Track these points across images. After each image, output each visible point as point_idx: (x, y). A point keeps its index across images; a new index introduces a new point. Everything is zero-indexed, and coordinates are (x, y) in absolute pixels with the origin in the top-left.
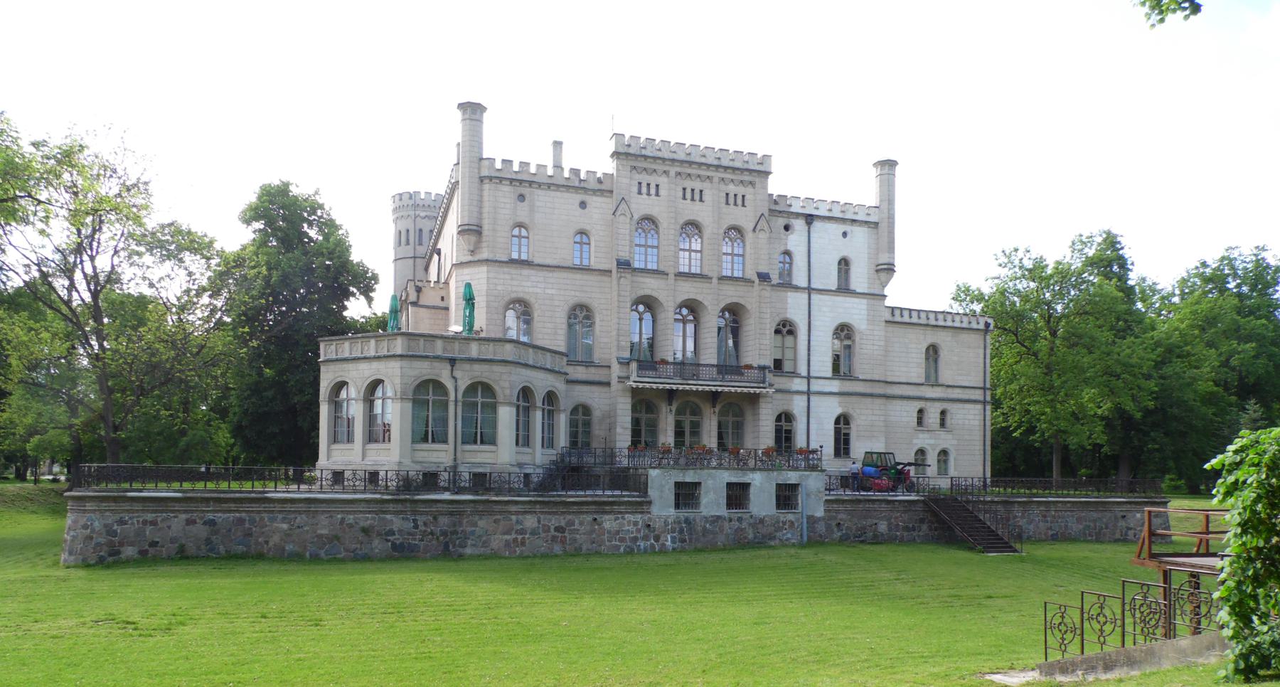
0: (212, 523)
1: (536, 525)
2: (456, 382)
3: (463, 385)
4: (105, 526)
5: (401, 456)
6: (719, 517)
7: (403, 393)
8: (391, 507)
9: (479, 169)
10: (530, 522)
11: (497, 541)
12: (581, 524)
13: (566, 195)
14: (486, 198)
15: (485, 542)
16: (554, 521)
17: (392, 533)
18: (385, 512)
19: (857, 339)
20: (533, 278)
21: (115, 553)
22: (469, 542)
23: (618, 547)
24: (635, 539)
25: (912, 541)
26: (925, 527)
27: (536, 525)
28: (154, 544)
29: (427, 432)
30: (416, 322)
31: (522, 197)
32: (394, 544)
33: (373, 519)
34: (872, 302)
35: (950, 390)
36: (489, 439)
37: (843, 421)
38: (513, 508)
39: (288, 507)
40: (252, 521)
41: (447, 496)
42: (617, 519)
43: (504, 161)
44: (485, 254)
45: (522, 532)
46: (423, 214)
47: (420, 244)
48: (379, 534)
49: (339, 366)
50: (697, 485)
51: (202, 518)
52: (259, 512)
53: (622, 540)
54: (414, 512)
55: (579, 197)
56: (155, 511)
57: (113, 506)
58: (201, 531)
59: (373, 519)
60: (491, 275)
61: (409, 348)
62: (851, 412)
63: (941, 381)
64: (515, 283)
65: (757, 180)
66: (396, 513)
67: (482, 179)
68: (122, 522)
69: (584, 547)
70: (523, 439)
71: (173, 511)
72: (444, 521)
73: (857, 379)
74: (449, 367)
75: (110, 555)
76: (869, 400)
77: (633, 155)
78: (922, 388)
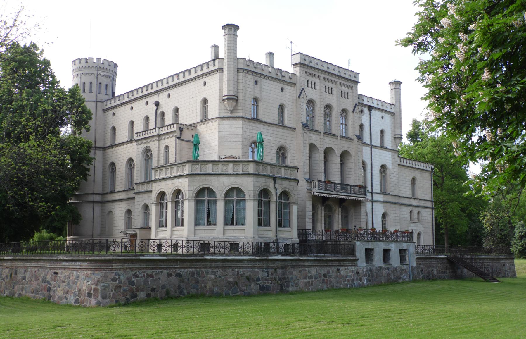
0: (179, 275)
1: (316, 273)
2: (220, 186)
3: (279, 192)
4: (128, 278)
5: (254, 234)
6: (381, 267)
7: (254, 196)
8: (258, 264)
9: (237, 63)
10: (313, 271)
11: (302, 282)
12: (333, 272)
13: (275, 83)
14: (240, 81)
15: (296, 284)
16: (323, 271)
17: (258, 279)
18: (255, 267)
19: (388, 173)
21: (135, 296)
22: (291, 284)
23: (347, 285)
24: (353, 280)
25: (444, 279)
26: (448, 271)
27: (316, 273)
28: (153, 290)
29: (233, 219)
30: (181, 150)
31: (256, 82)
32: (260, 286)
33: (250, 271)
34: (393, 154)
35: (420, 201)
38: (307, 264)
39: (214, 265)
40: (198, 273)
41: (279, 257)
42: (345, 269)
44: (240, 114)
45: (310, 277)
46: (102, 74)
47: (100, 93)
48: (254, 281)
50: (373, 249)
51: (174, 272)
52: (200, 268)
53: (348, 281)
54: (268, 267)
55: (281, 85)
56: (152, 269)
57: (131, 265)
58: (174, 280)
59: (250, 271)
60: (244, 126)
61: (256, 170)
62: (387, 212)
65: (353, 85)
66: (260, 267)
67: (238, 70)
68: (136, 276)
69: (335, 285)
70: (262, 220)
71: (161, 268)
72: (279, 271)
73: (389, 194)
74: (273, 182)
75: (132, 298)
76: (397, 206)
77: (308, 65)
78: (412, 200)
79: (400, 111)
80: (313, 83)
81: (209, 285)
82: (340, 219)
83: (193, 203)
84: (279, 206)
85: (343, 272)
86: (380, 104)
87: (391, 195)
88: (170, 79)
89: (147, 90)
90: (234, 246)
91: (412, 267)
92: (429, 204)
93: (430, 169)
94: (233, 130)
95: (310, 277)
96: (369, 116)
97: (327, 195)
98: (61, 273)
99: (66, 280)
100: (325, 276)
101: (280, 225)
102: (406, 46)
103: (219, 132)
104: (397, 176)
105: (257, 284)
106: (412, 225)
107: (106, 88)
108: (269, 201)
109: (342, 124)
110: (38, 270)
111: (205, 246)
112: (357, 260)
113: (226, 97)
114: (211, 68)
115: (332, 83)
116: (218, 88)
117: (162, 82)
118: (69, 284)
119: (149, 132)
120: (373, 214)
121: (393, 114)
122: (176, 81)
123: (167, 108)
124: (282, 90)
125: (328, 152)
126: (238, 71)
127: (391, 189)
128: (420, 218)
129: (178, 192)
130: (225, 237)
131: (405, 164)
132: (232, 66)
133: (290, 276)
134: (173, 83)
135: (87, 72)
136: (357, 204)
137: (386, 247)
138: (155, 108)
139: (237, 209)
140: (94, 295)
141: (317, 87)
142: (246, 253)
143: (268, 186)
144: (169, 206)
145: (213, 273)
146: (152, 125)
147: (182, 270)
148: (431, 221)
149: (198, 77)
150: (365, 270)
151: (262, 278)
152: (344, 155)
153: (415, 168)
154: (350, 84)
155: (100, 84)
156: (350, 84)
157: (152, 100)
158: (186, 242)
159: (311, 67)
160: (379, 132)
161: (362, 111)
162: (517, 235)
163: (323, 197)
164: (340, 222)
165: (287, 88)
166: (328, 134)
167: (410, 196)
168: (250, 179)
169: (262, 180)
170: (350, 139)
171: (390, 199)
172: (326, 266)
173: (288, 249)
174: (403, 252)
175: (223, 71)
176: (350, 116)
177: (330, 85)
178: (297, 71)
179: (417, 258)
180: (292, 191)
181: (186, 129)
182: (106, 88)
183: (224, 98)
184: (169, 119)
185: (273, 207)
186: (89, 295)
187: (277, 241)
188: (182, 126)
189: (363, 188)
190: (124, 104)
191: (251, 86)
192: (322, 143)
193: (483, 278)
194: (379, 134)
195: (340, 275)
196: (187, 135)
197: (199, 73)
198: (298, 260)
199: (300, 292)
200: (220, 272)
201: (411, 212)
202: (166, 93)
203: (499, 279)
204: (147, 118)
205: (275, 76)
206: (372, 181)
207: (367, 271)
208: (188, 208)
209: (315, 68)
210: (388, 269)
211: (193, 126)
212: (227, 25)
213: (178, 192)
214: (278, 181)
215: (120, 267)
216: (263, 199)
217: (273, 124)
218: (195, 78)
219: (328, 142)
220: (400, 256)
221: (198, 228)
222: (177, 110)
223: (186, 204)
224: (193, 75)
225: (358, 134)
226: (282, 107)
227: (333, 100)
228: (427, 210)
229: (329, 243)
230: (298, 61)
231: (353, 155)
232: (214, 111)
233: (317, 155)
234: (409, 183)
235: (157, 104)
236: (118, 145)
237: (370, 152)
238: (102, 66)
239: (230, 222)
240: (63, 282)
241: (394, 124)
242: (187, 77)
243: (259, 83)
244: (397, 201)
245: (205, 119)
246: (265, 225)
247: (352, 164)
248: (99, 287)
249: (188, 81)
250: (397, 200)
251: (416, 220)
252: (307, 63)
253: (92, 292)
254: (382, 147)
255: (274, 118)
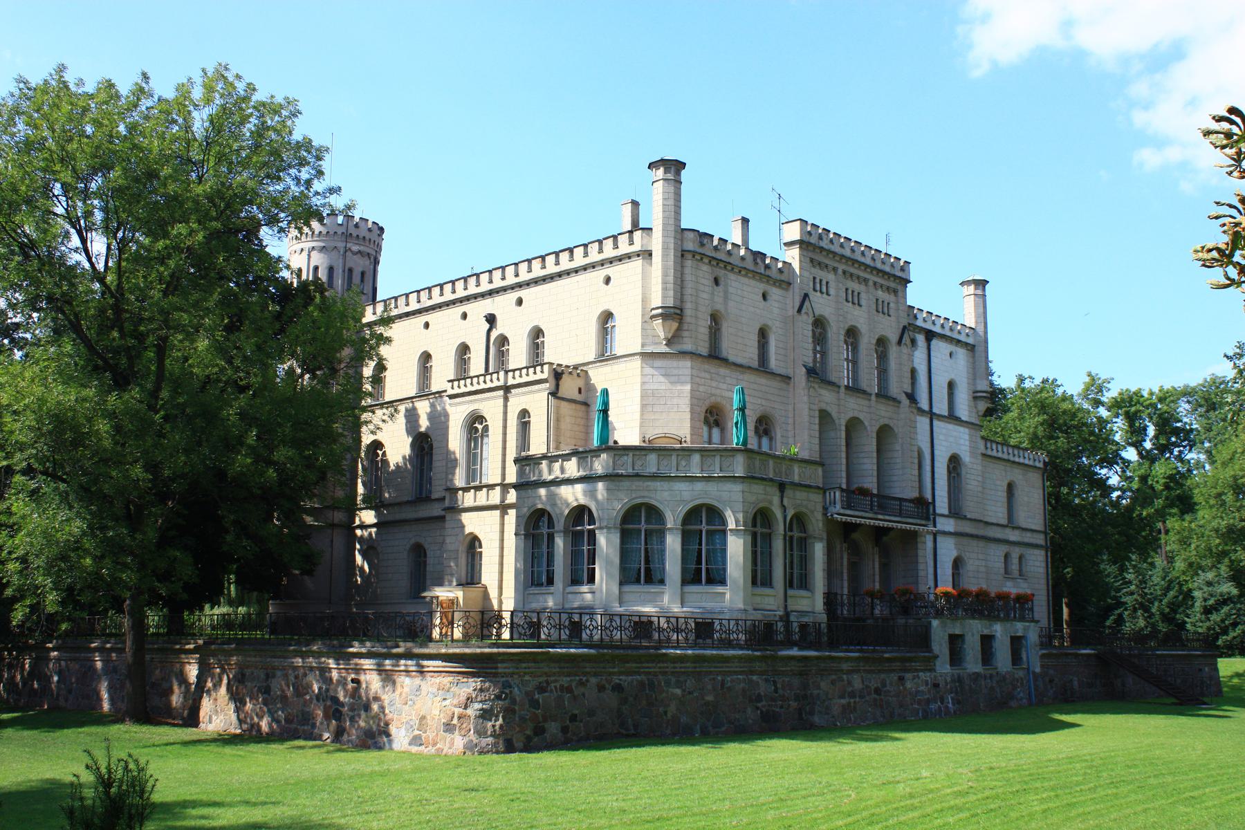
0: (618, 688)
2: (674, 502)
3: (790, 514)
4: (527, 694)
9: (682, 240)
13: (753, 282)
14: (688, 277)
17: (759, 698)
18: (752, 673)
20: (728, 380)
21: (539, 731)
24: (928, 702)
28: (573, 718)
31: (716, 281)
35: (1024, 534)
36: (717, 578)
37: (957, 564)
38: (845, 666)
41: (795, 652)
43: (720, 239)
45: (852, 695)
46: (355, 248)
49: (638, 484)
52: (655, 674)
53: (919, 703)
58: (611, 699)
61: (749, 467)
64: (714, 384)
70: (759, 576)
71: (585, 674)
73: (965, 518)
76: (981, 544)
77: (816, 245)
78: (1008, 531)
79: (986, 341)
80: (824, 283)
81: (672, 709)
83: (616, 538)
84: (789, 542)
86: (947, 326)
87: (970, 520)
89: (466, 289)
90: (704, 629)
91: (1034, 673)
92: (1040, 539)
93: (1041, 465)
95: (852, 695)
96: (926, 351)
97: (858, 520)
100: (877, 691)
101: (791, 586)
102: (1207, 264)
103: (643, 383)
104: (980, 479)
106: (1009, 584)
107: (362, 280)
109: (847, 359)
112: (937, 657)
113: (660, 311)
114: (624, 248)
116: (639, 291)
119: (469, 381)
120: (941, 562)
121: (971, 348)
123: (515, 326)
124: (764, 297)
127: (971, 510)
131: (994, 453)
132: (672, 246)
136: (911, 538)
137: (986, 632)
138: (487, 326)
139: (708, 551)
140: (460, 729)
141: (832, 291)
142: (729, 644)
143: (771, 502)
145: (679, 684)
146: (476, 365)
147: (623, 677)
148: (1044, 576)
149: (593, 266)
150: (949, 679)
152: (884, 433)
153: (1014, 462)
154: (892, 285)
156: (892, 285)
157: (478, 310)
158: (461, 614)
159: (822, 249)
160: (946, 386)
162: (1198, 605)
165: (775, 293)
166: (855, 389)
167: (1004, 522)
168: (737, 488)
169: (758, 488)
170: (894, 400)
171: (967, 528)
172: (880, 671)
173: (807, 635)
174: (1016, 642)
175: (651, 255)
176: (893, 351)
177: (854, 285)
178: (793, 257)
179: (1043, 656)
182: (362, 280)
183: (654, 312)
184: (518, 355)
186: (449, 728)
187: (786, 618)
188: (559, 370)
189: (923, 507)
190: (407, 315)
191: (707, 289)
193: (1176, 697)
194: (945, 391)
195: (905, 689)
196: (569, 387)
198: (831, 658)
202: (513, 296)
203: (1205, 699)
204: (464, 349)
207: (953, 681)
209: (829, 251)
210: (991, 676)
212: (662, 160)
215: (511, 670)
216: (759, 530)
217: (749, 368)
218: (585, 268)
219: (853, 407)
221: (627, 588)
222: (537, 333)
225: (909, 391)
226: (763, 334)
227: (859, 317)
228: (1037, 552)
229: (869, 621)
230: (797, 237)
232: (628, 336)
233: (832, 434)
234: (1002, 495)
235: (491, 319)
237: (928, 427)
238: (354, 232)
239: (692, 576)
241: (974, 368)
243: (722, 282)
244: (977, 534)
245: (605, 356)
249: (568, 273)
250: (981, 531)
251: (1016, 573)
252: (813, 240)
253: (455, 721)
254: (952, 417)
255: (749, 355)
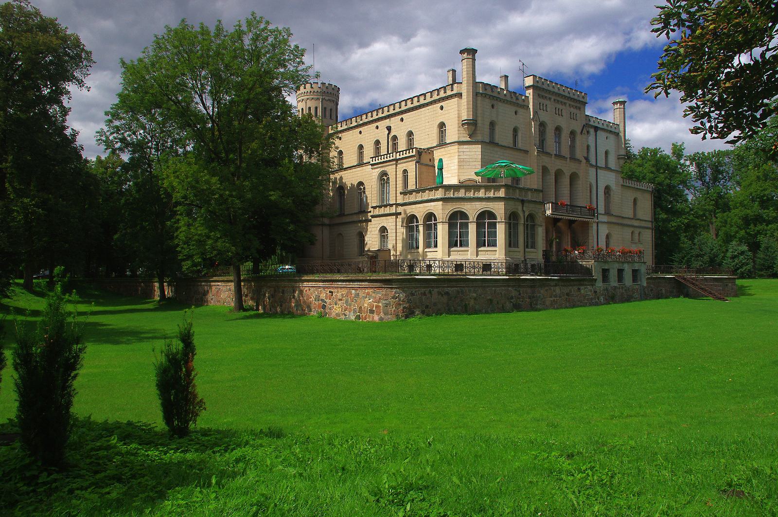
0: (447, 293)
2: (472, 210)
3: (527, 214)
10: (558, 290)
14: (479, 105)
16: (566, 290)
17: (512, 298)
18: (509, 286)
22: (539, 302)
26: (675, 290)
31: (493, 106)
42: (585, 288)
45: (556, 296)
46: (327, 98)
52: (464, 287)
55: (514, 109)
56: (425, 287)
63: (638, 217)
65: (582, 106)
66: (513, 287)
74: (521, 205)
78: (633, 221)
82: (569, 240)
83: (447, 226)
84: (526, 227)
85: (582, 291)
87: (615, 216)
88: (403, 103)
90: (487, 267)
91: (643, 286)
92: (649, 225)
94: (473, 153)
95: (556, 296)
98: (338, 292)
99: (344, 298)
100: (568, 294)
101: (527, 247)
105: (511, 302)
106: (634, 245)
108: (517, 223)
110: (310, 290)
111: (459, 267)
114: (449, 93)
115: (562, 105)
117: (394, 107)
118: (347, 302)
122: (409, 105)
124: (516, 113)
125: (558, 174)
126: (476, 95)
127: (615, 210)
128: (641, 238)
129: (430, 216)
130: (478, 258)
133: (538, 295)
134: (407, 107)
135: (312, 97)
143: (517, 209)
144: (421, 228)
146: (383, 151)
150: (601, 289)
151: (515, 296)
155: (325, 108)
161: (588, 132)
163: (570, 220)
164: (569, 243)
167: (632, 216)
169: (511, 203)
171: (613, 220)
176: (579, 139)
177: (559, 106)
179: (648, 279)
180: (537, 213)
181: (424, 153)
184: (402, 145)
185: (521, 229)
189: (592, 211)
190: (352, 128)
192: (553, 165)
196: (425, 158)
197: (435, 97)
199: (546, 308)
200: (480, 291)
201: (632, 233)
204: (377, 143)
205: (509, 99)
206: (597, 202)
208: (442, 231)
209: (547, 90)
211: (430, 151)
212: (466, 49)
213: (430, 216)
214: (526, 204)
216: (529, 223)
217: (509, 147)
219: (558, 164)
220: (633, 275)
222: (410, 134)
223: (440, 227)
224: (429, 99)
227: (563, 122)
228: (647, 230)
231: (581, 177)
234: (631, 204)
235: (389, 129)
236: (346, 169)
240: (340, 300)
242: (422, 101)
246: (532, 247)
247: (581, 185)
248: (380, 304)
250: (621, 221)
251: (637, 241)
254: (607, 168)
